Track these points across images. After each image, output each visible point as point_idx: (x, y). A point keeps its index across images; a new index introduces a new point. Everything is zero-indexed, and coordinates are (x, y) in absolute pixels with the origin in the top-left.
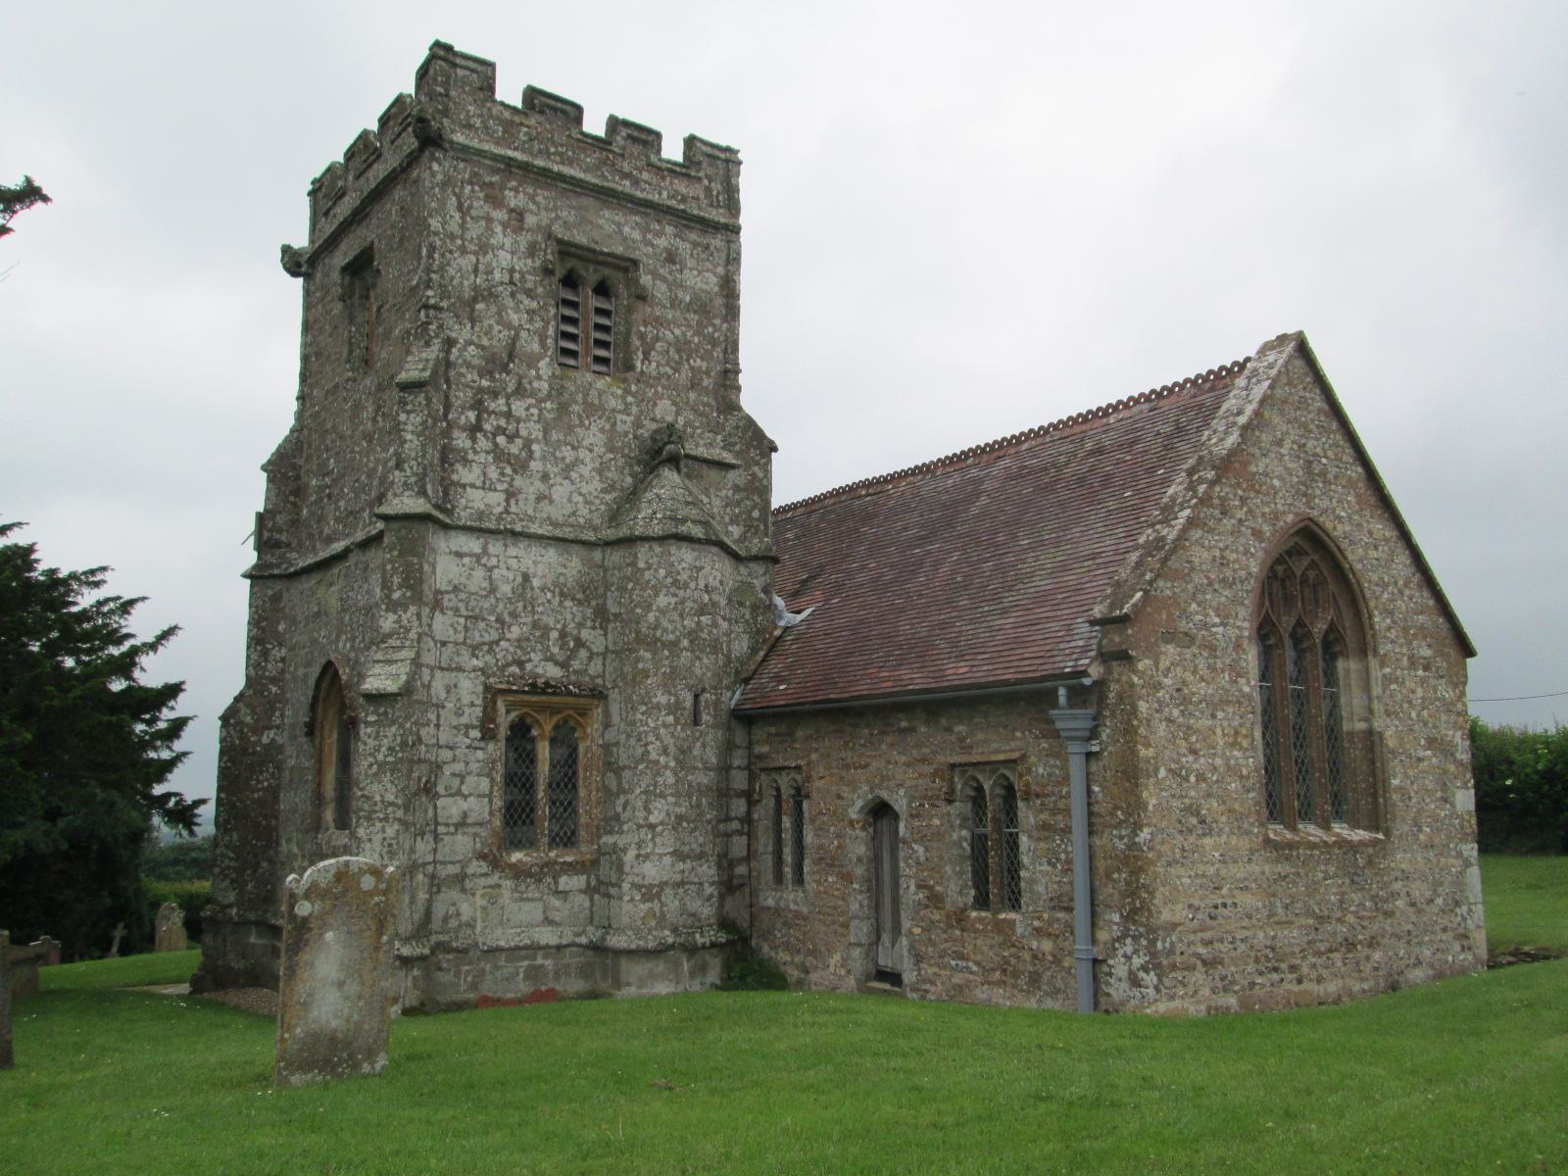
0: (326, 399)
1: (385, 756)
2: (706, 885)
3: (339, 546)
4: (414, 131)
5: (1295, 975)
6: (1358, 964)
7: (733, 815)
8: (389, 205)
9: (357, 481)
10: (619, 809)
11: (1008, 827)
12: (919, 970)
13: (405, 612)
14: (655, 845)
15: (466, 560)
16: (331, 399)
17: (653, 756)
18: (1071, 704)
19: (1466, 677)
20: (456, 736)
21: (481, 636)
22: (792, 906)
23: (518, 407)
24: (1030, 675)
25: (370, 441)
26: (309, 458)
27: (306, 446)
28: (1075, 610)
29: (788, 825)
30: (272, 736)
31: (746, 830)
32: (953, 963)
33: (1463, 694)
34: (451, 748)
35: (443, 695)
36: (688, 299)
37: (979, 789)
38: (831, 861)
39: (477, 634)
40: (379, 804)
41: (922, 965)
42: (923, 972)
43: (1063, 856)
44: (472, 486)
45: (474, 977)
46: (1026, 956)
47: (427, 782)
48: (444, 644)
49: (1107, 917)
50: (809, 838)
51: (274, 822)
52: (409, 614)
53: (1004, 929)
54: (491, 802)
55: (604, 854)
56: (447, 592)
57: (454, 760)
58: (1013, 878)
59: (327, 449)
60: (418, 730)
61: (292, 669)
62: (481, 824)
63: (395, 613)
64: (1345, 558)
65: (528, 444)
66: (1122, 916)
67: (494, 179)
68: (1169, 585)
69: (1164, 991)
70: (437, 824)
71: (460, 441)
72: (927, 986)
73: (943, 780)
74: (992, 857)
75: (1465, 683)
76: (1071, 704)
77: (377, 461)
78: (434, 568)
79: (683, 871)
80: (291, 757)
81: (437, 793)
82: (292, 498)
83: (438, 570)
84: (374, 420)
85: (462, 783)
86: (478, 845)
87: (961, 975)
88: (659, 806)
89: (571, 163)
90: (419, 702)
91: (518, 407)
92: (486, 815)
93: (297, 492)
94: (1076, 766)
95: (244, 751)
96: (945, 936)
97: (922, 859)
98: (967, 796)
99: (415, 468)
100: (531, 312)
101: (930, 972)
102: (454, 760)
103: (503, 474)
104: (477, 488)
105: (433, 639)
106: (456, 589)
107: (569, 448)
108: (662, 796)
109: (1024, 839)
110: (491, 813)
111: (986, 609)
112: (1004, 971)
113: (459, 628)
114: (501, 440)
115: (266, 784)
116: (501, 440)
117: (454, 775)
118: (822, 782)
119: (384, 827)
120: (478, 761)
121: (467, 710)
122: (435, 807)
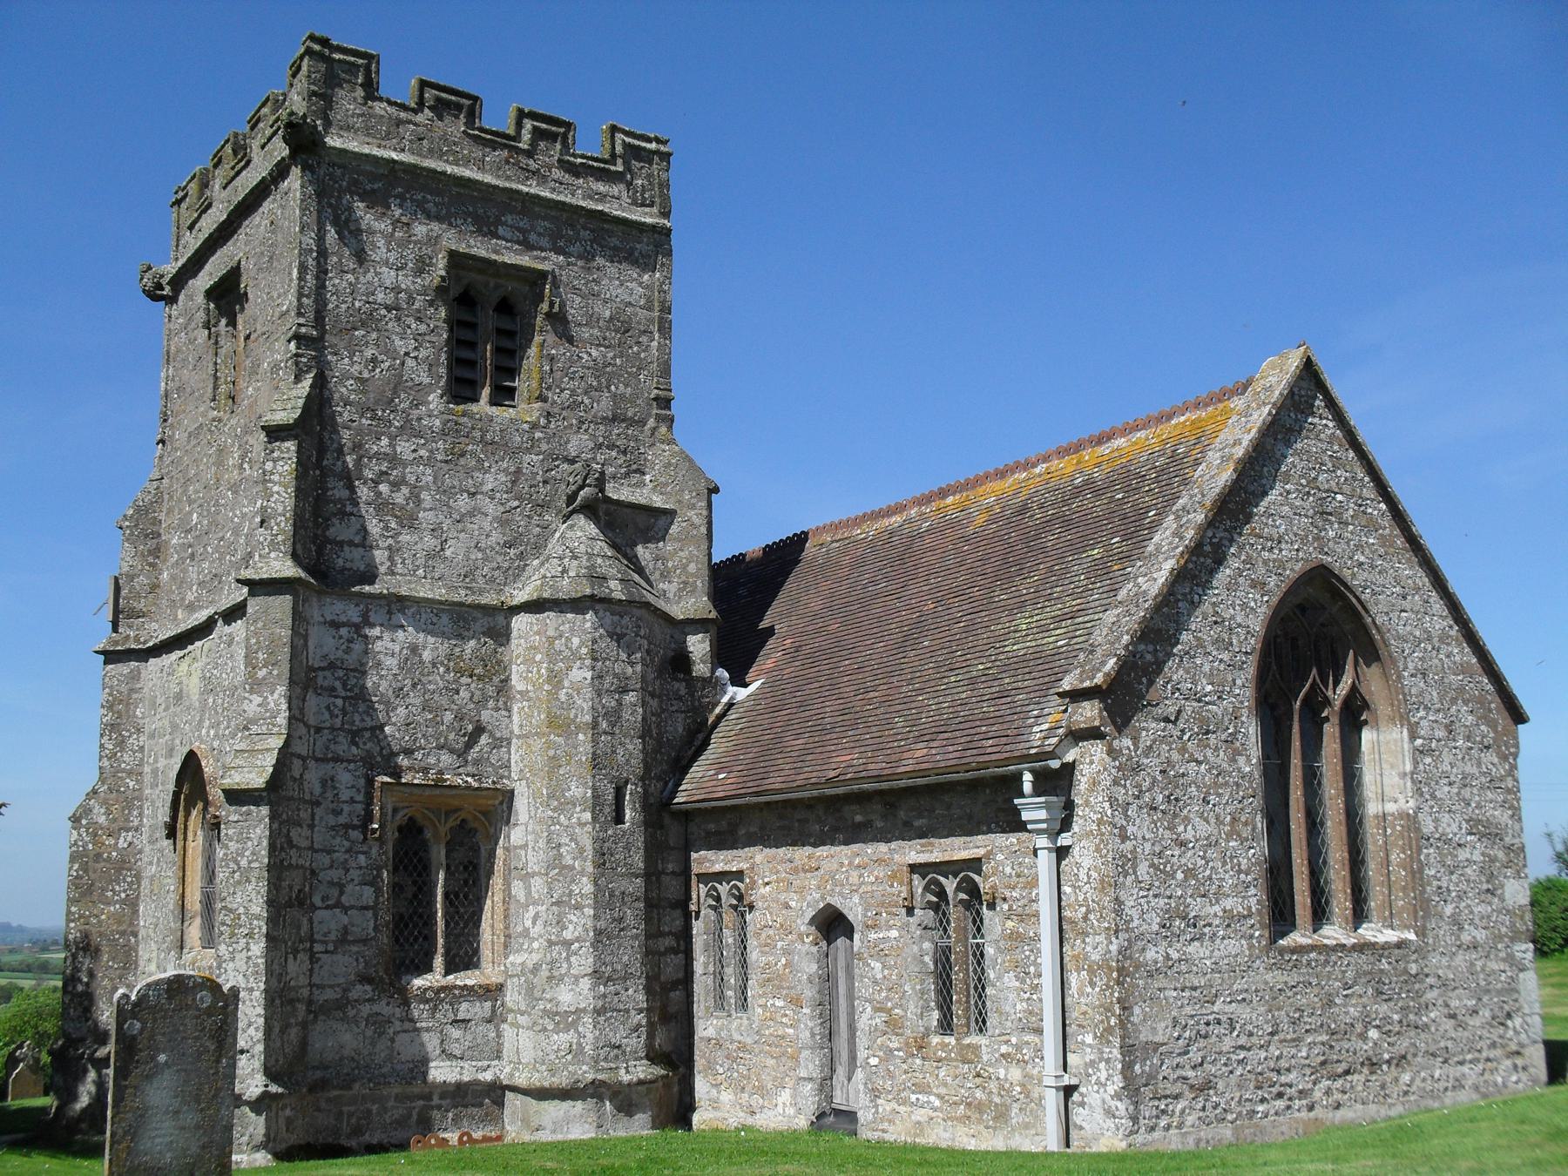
0: (189, 442)
1: (250, 862)
2: (633, 1013)
3: (202, 616)
4: (284, 137)
5: (1304, 1102)
6: (1383, 1087)
7: (667, 929)
8: (258, 219)
9: (222, 539)
10: (528, 923)
11: (974, 937)
12: (876, 1106)
13: (272, 693)
14: (570, 966)
15: (344, 631)
16: (193, 442)
17: (568, 860)
18: (1037, 792)
19: (1517, 746)
20: (334, 838)
21: (363, 720)
22: (736, 1037)
23: (404, 448)
24: (994, 757)
25: (235, 492)
26: (170, 511)
27: (166, 497)
28: (1046, 679)
29: (730, 940)
30: (129, 839)
31: (682, 948)
32: (913, 1097)
33: (1514, 767)
34: (329, 852)
35: (317, 790)
36: (608, 314)
37: (942, 894)
38: (774, 982)
39: (357, 718)
40: (243, 917)
41: (880, 1101)
42: (880, 1110)
43: (1032, 969)
44: (351, 543)
45: (359, 1119)
46: (993, 1086)
47: (300, 891)
48: (318, 730)
49: (1080, 1038)
50: (754, 955)
51: (133, 940)
52: (276, 696)
53: (968, 1055)
54: (375, 916)
55: (511, 976)
56: (322, 669)
57: (332, 867)
58: (980, 997)
59: (190, 502)
60: (289, 831)
61: (151, 761)
62: (365, 941)
63: (259, 694)
64: (1367, 611)
65: (415, 497)
66: (1095, 1037)
67: (376, 186)
68: (1151, 648)
69: (1142, 1122)
70: (313, 941)
71: (336, 491)
72: (885, 1125)
73: (901, 884)
74: (956, 974)
75: (1515, 756)
76: (1037, 792)
77: (244, 515)
78: (306, 641)
79: (605, 996)
80: (151, 863)
81: (313, 905)
82: (151, 559)
83: (310, 643)
84: (241, 467)
85: (342, 893)
86: (361, 966)
87: (923, 1111)
88: (574, 919)
89: (466, 162)
90: (291, 799)
91: (404, 448)
92: (371, 931)
93: (156, 552)
94: (1045, 861)
95: (98, 856)
96: (905, 1066)
97: (879, 976)
98: (928, 902)
99: (283, 524)
100: (418, 337)
101: (888, 1108)
102: (332, 867)
103: (386, 528)
104: (357, 546)
105: (306, 725)
106: (332, 666)
107: (465, 495)
108: (578, 907)
109: (990, 951)
110: (376, 928)
111: (953, 679)
112: (969, 1104)
113: (336, 711)
114: (383, 488)
115: (123, 895)
116: (384, 488)
117: (331, 883)
118: (768, 888)
119: (248, 943)
120: (361, 868)
121: (346, 808)
122: (311, 921)
